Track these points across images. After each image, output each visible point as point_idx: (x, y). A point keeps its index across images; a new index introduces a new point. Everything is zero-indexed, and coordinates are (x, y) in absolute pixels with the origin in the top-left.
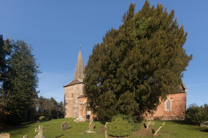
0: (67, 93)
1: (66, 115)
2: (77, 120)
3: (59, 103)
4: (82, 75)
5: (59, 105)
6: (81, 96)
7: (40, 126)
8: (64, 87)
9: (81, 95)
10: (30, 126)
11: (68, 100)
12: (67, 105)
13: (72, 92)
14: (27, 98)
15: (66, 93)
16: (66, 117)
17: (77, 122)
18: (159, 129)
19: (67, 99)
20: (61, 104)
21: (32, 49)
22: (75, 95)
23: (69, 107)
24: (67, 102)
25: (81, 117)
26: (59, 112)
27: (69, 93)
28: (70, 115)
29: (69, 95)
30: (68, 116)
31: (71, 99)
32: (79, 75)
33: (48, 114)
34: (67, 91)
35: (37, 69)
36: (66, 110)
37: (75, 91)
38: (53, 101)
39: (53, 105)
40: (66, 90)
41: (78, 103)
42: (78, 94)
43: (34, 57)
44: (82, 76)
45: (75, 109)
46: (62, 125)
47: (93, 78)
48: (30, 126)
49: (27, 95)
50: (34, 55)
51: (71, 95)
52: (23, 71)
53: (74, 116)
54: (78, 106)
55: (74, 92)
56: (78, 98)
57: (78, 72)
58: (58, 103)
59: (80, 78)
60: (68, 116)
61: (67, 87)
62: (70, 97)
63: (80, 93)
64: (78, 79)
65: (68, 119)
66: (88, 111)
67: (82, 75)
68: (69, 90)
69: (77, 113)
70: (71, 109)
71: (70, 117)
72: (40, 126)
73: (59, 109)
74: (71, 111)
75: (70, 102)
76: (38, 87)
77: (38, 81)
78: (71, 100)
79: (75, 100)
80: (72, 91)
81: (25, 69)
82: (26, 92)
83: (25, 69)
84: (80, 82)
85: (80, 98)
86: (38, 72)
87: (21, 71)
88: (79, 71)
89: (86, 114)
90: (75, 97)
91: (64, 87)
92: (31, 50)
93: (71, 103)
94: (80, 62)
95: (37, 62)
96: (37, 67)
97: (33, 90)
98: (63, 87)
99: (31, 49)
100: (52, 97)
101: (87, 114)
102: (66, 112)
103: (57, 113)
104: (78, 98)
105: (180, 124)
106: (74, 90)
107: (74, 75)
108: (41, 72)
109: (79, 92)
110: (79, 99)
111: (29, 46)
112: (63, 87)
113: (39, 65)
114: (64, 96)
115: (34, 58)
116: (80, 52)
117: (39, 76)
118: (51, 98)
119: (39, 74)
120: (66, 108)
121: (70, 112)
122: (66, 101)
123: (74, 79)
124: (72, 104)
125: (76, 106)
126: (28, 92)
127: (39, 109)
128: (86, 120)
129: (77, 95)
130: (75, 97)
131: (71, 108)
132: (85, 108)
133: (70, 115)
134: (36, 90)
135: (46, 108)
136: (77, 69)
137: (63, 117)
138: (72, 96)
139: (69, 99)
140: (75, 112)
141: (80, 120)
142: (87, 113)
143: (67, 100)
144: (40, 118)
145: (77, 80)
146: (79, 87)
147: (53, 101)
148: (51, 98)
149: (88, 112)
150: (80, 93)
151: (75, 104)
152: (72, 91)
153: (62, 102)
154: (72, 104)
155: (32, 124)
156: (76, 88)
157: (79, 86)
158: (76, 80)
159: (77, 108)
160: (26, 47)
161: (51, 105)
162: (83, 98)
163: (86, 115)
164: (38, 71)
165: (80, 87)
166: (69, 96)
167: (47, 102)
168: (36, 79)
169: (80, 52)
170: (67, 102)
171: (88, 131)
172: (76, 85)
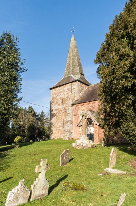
0: (55, 98)
1: (52, 133)
2: (78, 144)
3: (39, 114)
4: (76, 69)
5: (40, 118)
6: (77, 102)
7: (42, 161)
8: (51, 89)
9: (77, 100)
10: (8, 155)
11: (56, 110)
12: (55, 118)
13: (62, 97)
14: (7, 109)
15: (53, 98)
16: (52, 137)
17: (77, 148)
19: (55, 107)
20: (41, 116)
21: (18, 41)
22: (67, 101)
23: (58, 120)
24: (53, 112)
25: (84, 138)
26: (39, 129)
27: (58, 97)
28: (59, 135)
29: (57, 100)
30: (56, 135)
31: (61, 107)
32: (72, 69)
33: (24, 132)
34: (54, 96)
35: (22, 67)
36: (52, 126)
37: (67, 94)
38: (31, 112)
39: (31, 118)
40: (53, 94)
41: (72, 113)
42: (72, 98)
43: (19, 51)
44: (76, 71)
45: (68, 124)
46: (61, 156)
47: (124, 67)
48: (8, 155)
49: (7, 105)
50: (19, 49)
51: (60, 101)
52: (5, 71)
53: (66, 136)
54: (72, 119)
55: (66, 96)
56: (73, 105)
57: (71, 65)
58: (37, 114)
59: (73, 73)
60: (56, 135)
61: (55, 89)
62: (59, 104)
63: (75, 96)
64: (71, 75)
65: (59, 142)
67: (76, 69)
68: (58, 93)
69: (71, 131)
70: (60, 124)
71: (59, 137)
72: (42, 161)
73: (39, 123)
74: (61, 128)
75: (59, 113)
76: (21, 92)
77: (21, 83)
78: (61, 109)
79: (66, 108)
80: (63, 94)
81: (8, 68)
82: (7, 100)
83: (8, 68)
84: (74, 80)
85: (74, 105)
86: (22, 71)
87: (3, 71)
88: (72, 64)
90: (67, 104)
91: (51, 89)
92: (17, 42)
93: (61, 114)
94: (72, 51)
95: (22, 58)
96: (22, 64)
97: (14, 97)
98: (50, 89)
99: (17, 41)
100: (30, 106)
102: (53, 128)
103: (36, 130)
104: (73, 105)
106: (65, 93)
107: (66, 69)
108: (26, 70)
109: (73, 95)
110: (73, 107)
111: (15, 37)
112: (50, 89)
113: (24, 61)
114: (51, 102)
115: (19, 52)
116: (73, 37)
117: (23, 75)
118: (30, 107)
119: (23, 73)
120: (53, 122)
121: (59, 128)
122: (52, 111)
123: (65, 75)
124: (62, 116)
125: (69, 119)
126: (8, 100)
127: (13, 125)
128: (92, 144)
129: (71, 101)
130: (67, 104)
131: (61, 122)
133: (59, 135)
134: (17, 95)
135: (22, 123)
136: (70, 62)
137: (48, 137)
138: (63, 103)
139: (57, 108)
140: (68, 128)
141: (84, 145)
143: (55, 109)
144: (16, 140)
145: (69, 77)
146: (72, 88)
147: (31, 112)
148: (30, 107)
150: (75, 96)
151: (68, 115)
152: (63, 94)
153: (43, 112)
154: (62, 116)
155: (9, 150)
156: (68, 89)
157: (72, 85)
158: (68, 77)
159: (70, 121)
160: (12, 39)
161: (29, 119)
162: (79, 104)
163: (87, 135)
164: (23, 70)
166: (58, 103)
167: (24, 114)
168: (19, 80)
169: (73, 37)
170: (53, 112)
172: (69, 84)
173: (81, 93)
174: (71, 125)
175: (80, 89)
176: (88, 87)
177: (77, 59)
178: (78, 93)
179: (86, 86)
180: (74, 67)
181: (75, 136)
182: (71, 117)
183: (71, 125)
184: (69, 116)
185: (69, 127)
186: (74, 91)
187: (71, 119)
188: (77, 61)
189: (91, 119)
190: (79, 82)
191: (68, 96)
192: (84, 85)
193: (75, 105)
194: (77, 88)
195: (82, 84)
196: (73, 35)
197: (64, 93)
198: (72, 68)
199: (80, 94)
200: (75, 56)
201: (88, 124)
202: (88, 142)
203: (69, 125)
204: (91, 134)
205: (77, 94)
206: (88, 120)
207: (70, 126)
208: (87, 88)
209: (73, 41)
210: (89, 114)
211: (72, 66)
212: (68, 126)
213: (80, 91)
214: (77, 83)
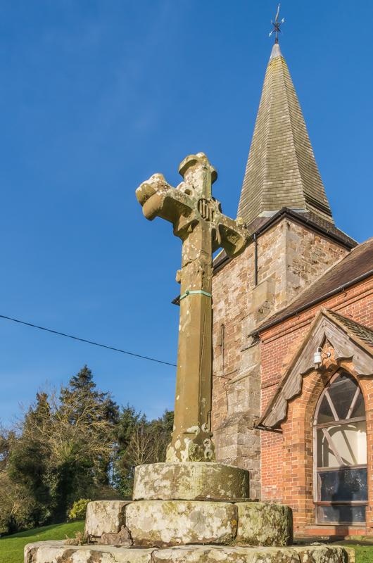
18: (352, 406)
32: (269, 189)
41: (253, 375)
44: (287, 191)
56: (256, 336)
57: (265, 170)
63: (271, 297)
66: (343, 428)
67: (287, 184)
88: (269, 166)
89: (322, 462)
101: (334, 463)
105: (364, 402)
106: (232, 296)
109: (261, 293)
110: (259, 348)
116: (276, 52)
132: (306, 393)
142: (324, 447)
146: (262, 261)
149: (336, 440)
151: (232, 390)
163: (325, 477)
165: (269, 253)
169: (276, 52)
171: (353, 502)
173: (304, 277)
174: (244, 438)
175: (300, 257)
176: (347, 253)
177: (295, 142)
178: (288, 278)
179: (338, 249)
180: (280, 178)
181: (267, 490)
182: (247, 396)
183: (244, 438)
184: (239, 392)
185: (235, 446)
186: (270, 272)
187: (246, 404)
188: (292, 149)
189: (345, 373)
190: (293, 225)
191: (242, 306)
192: (325, 244)
193: (270, 333)
194: (283, 255)
195: (311, 235)
196: (277, 46)
197: (226, 301)
198: (266, 184)
199: (302, 283)
200: (281, 132)
201: (325, 410)
202: (199, 518)
203: (235, 438)
204: (345, 471)
205: (280, 287)
206: (327, 384)
207: (240, 443)
208: (341, 258)
209: (276, 70)
210: (329, 337)
211: (269, 176)
212: (229, 443)
213: (296, 269)
214: (285, 227)
